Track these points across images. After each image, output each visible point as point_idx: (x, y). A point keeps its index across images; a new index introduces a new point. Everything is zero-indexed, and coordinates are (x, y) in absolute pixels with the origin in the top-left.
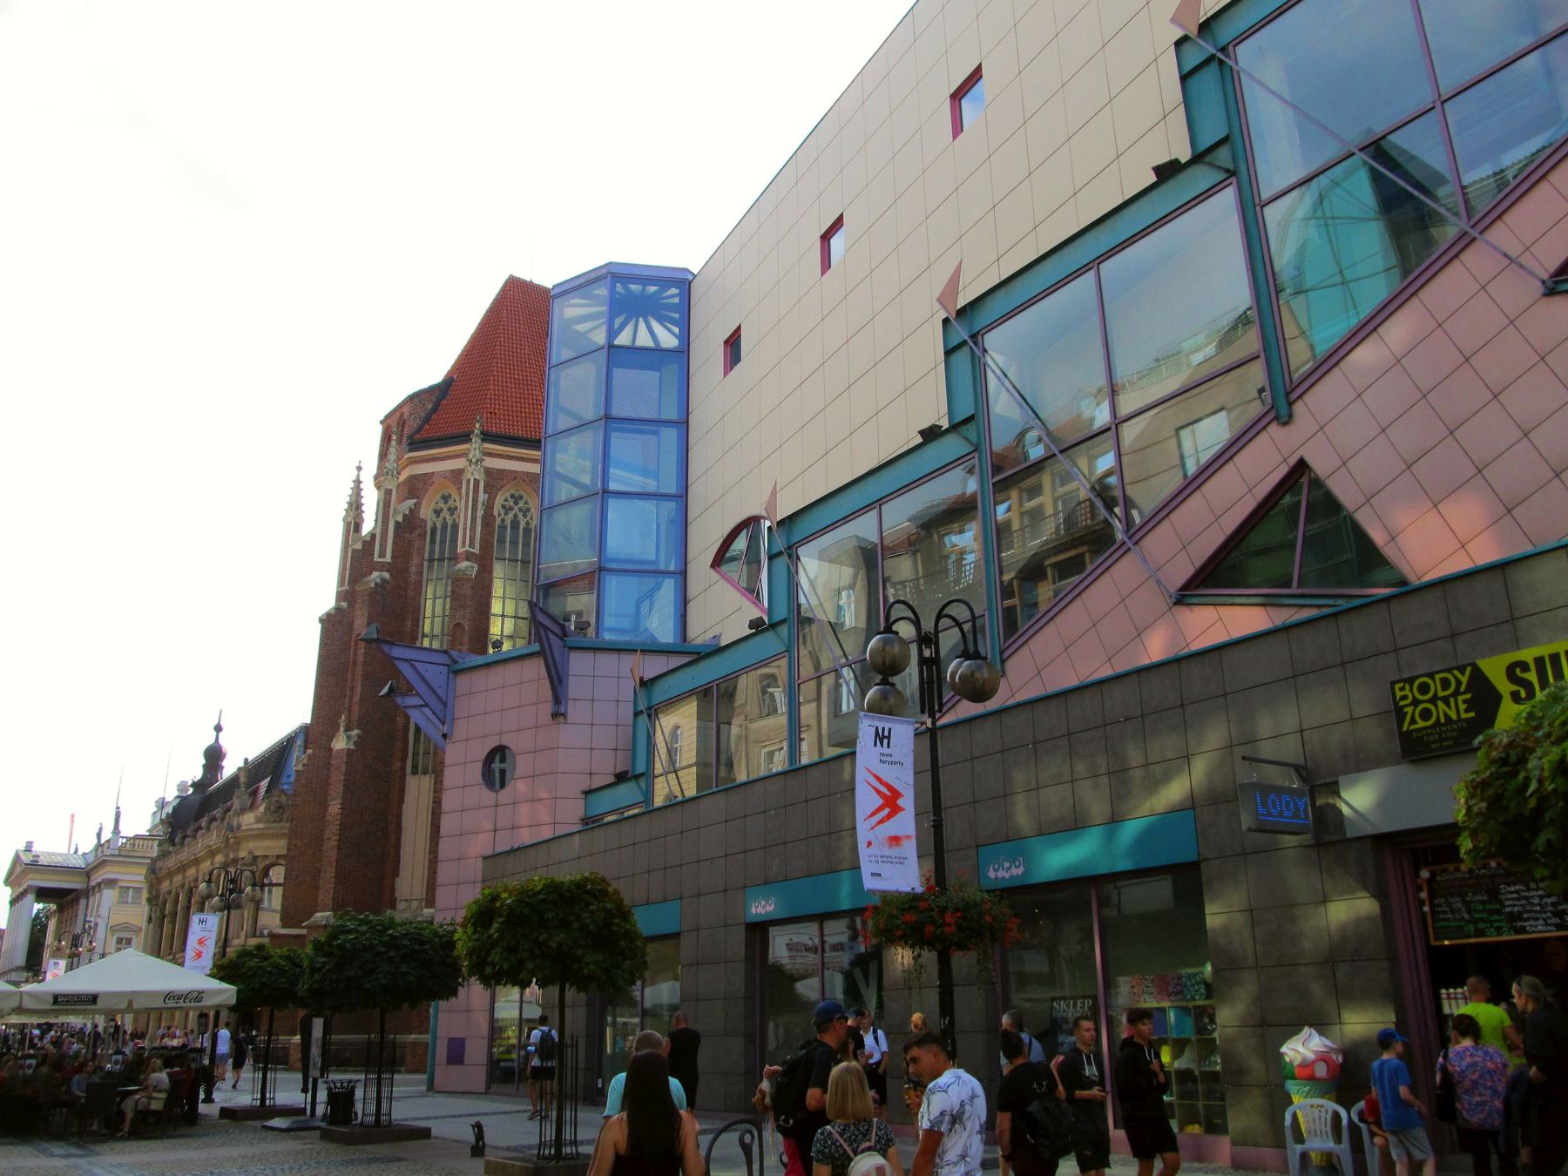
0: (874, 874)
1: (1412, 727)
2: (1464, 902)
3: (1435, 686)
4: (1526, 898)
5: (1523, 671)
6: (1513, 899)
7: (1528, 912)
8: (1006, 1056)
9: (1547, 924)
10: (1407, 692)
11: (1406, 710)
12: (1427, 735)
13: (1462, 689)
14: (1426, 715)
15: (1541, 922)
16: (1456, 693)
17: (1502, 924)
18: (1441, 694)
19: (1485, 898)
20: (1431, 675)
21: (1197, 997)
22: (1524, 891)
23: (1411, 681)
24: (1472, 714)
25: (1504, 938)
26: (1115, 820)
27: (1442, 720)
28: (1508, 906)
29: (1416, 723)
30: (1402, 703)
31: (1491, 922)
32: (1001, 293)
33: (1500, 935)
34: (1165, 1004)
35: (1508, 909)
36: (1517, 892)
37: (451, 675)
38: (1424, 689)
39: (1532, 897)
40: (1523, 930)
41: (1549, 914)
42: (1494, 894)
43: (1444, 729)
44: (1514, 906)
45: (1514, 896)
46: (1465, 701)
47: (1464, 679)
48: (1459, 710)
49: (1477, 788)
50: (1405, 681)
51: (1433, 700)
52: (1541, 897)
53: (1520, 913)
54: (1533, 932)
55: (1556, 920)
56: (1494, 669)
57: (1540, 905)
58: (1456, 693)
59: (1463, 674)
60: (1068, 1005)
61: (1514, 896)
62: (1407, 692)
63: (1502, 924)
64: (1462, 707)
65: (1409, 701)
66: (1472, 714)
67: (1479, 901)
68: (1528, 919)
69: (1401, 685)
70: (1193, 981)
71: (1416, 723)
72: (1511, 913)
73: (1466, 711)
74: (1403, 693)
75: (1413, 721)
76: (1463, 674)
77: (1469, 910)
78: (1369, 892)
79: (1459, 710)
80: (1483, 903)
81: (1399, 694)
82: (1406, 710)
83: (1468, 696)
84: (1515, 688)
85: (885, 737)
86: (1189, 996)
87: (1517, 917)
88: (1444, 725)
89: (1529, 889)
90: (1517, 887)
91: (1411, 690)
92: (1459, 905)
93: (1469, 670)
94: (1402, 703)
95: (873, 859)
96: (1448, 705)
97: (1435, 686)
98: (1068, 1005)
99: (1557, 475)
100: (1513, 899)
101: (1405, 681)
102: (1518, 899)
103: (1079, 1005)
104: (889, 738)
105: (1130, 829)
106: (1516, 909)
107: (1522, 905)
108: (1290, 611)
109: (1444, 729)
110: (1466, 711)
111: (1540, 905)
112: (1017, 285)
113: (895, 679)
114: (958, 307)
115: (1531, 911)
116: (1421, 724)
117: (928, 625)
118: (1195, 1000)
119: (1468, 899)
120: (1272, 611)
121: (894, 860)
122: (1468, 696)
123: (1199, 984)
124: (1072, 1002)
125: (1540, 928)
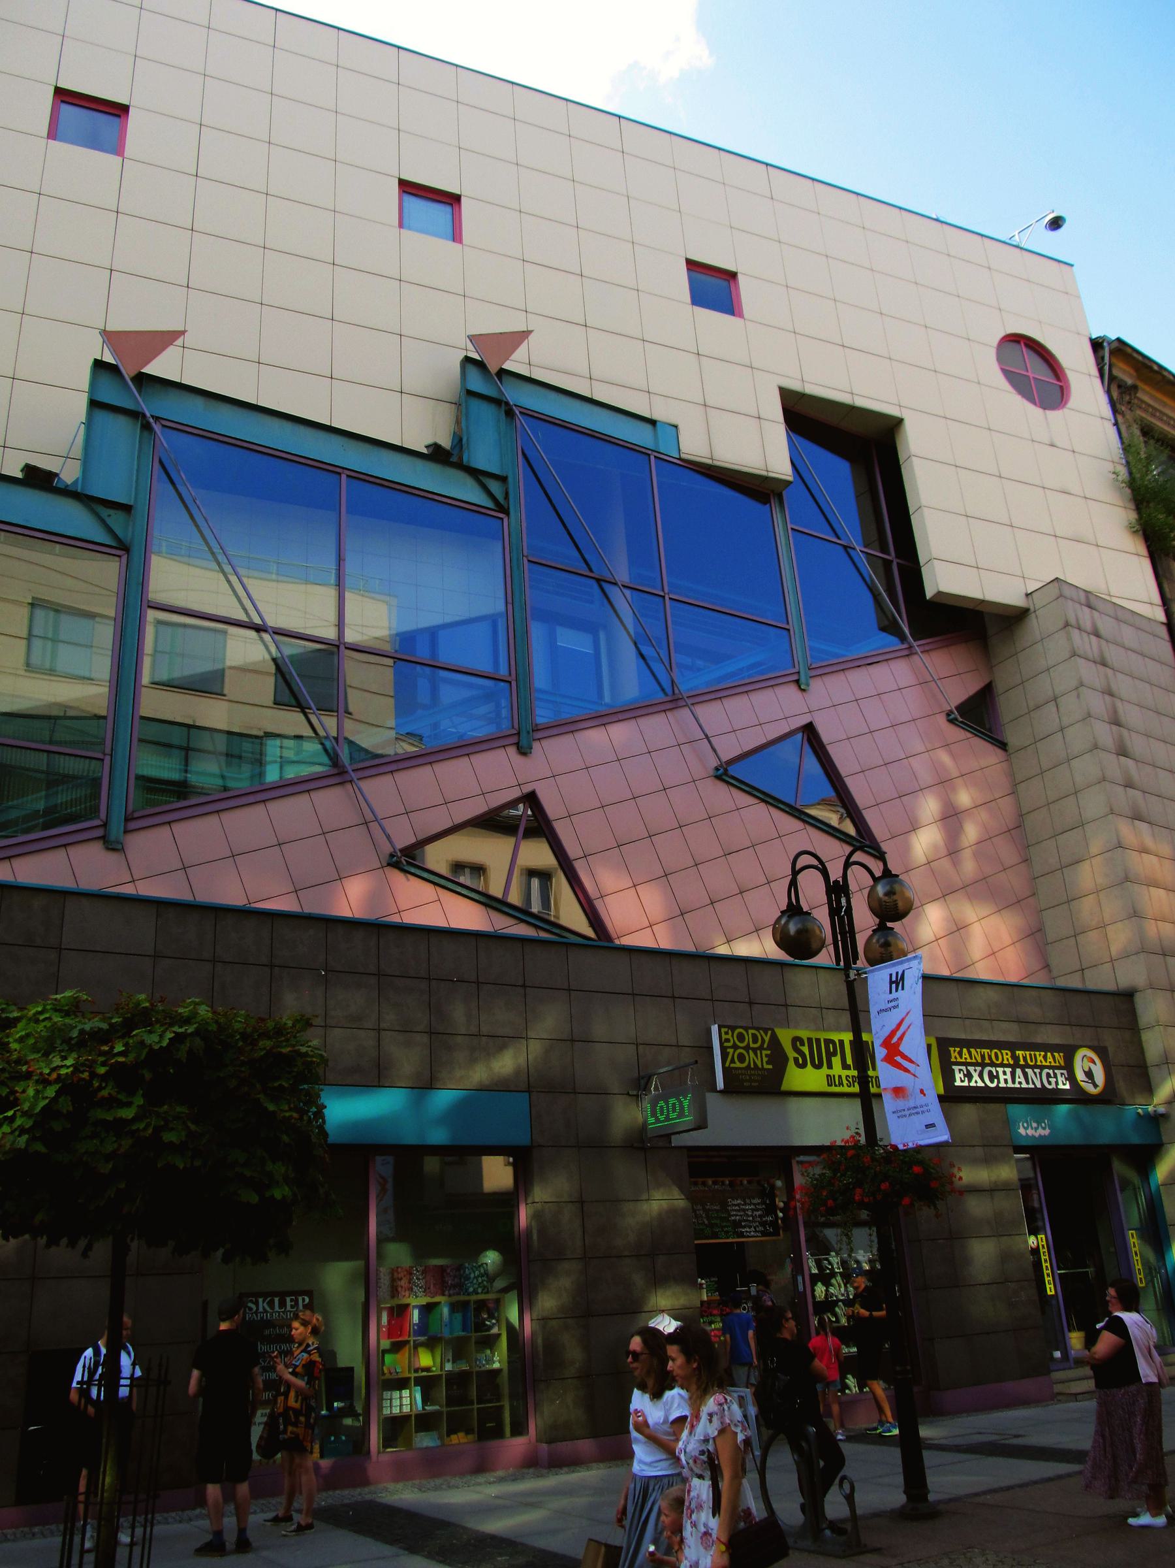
0: (932, 1125)
1: (732, 1065)
2: (704, 1210)
3: (748, 1038)
4: (744, 1210)
5: (801, 1045)
6: (735, 1210)
7: (745, 1221)
8: (1128, 1309)
9: (756, 1231)
10: (729, 1036)
11: (728, 1050)
12: (742, 1075)
13: (765, 1046)
14: (742, 1058)
15: (753, 1229)
16: (761, 1048)
17: (730, 1229)
18: (752, 1045)
19: (718, 1208)
20: (746, 1029)
21: (480, 1290)
22: (743, 1205)
23: (733, 1028)
24: (770, 1067)
25: (730, 1240)
26: (426, 1084)
27: (752, 1066)
28: (733, 1215)
29: (735, 1063)
30: (726, 1044)
31: (722, 1227)
32: (199, 401)
33: (728, 1238)
34: (437, 1299)
35: (733, 1218)
36: (738, 1205)
38: (741, 1038)
39: (747, 1210)
40: (741, 1235)
41: (757, 1224)
42: (724, 1206)
43: (753, 1072)
44: (737, 1215)
45: (737, 1208)
46: (767, 1056)
47: (767, 1039)
48: (761, 1060)
49: (143, 1096)
50: (728, 1027)
51: (747, 1048)
52: (753, 1210)
53: (740, 1221)
54: (749, 1237)
55: (761, 1228)
56: (785, 1036)
57: (752, 1216)
58: (761, 1048)
59: (766, 1035)
60: (271, 1304)
61: (737, 1208)
62: (729, 1036)
63: (730, 1229)
64: (765, 1059)
65: (730, 1044)
66: (770, 1067)
67: (715, 1210)
68: (744, 1227)
69: (726, 1030)
70: (477, 1273)
71: (735, 1063)
72: (734, 1221)
73: (768, 1063)
74: (727, 1037)
75: (733, 1061)
76: (766, 1035)
77: (708, 1217)
78: (685, 1195)
79: (761, 1060)
80: (717, 1211)
81: (724, 1037)
82: (728, 1050)
83: (769, 1052)
84: (797, 1056)
85: (894, 982)
86: (471, 1289)
87: (737, 1224)
88: (753, 1069)
89: (745, 1204)
90: (739, 1202)
91: (733, 1036)
92: (701, 1212)
93: (770, 1032)
94: (726, 1044)
95: (925, 1108)
96: (756, 1054)
97: (748, 1038)
98: (271, 1304)
99: (712, 903)
100: (735, 1210)
101: (728, 1027)
102: (739, 1211)
103: (289, 1303)
104: (891, 982)
105: (443, 1098)
106: (738, 1217)
107: (741, 1215)
108: (512, 921)
109: (753, 1072)
110: (768, 1063)
111: (752, 1216)
112: (226, 411)
113: (896, 926)
114: (145, 370)
115: (747, 1221)
116: (738, 1065)
117: (835, 874)
118: (477, 1293)
119: (708, 1207)
120: (495, 915)
121: (907, 1113)
122: (769, 1052)
123: (483, 1276)
124: (276, 1300)
125: (753, 1233)
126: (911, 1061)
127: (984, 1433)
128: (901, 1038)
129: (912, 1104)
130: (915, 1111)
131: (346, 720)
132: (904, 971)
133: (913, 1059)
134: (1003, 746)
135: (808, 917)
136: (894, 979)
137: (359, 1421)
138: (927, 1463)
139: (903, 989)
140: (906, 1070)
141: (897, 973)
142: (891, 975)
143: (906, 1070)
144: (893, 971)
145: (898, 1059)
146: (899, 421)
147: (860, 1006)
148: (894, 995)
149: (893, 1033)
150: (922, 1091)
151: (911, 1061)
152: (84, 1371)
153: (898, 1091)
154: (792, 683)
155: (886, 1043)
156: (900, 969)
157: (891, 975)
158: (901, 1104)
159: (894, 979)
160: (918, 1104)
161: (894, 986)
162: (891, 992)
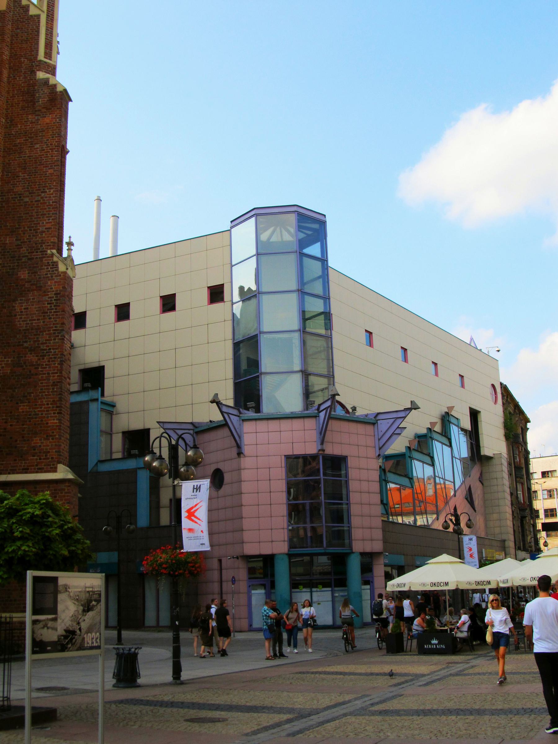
37: (241, 421)
104: (194, 488)
117: (174, 442)
126: (199, 519)
127: (296, 673)
128: (196, 510)
129: (196, 535)
130: (196, 538)
131: (248, 427)
132: (200, 485)
133: (201, 519)
134: (483, 484)
135: (163, 460)
136: (195, 487)
137: (65, 642)
138: (546, 705)
139: (200, 491)
140: (196, 522)
141: (197, 485)
142: (194, 486)
143: (196, 522)
144: (195, 484)
145: (193, 518)
146: (480, 412)
147: (461, 549)
148: (470, 542)
149: (192, 508)
150: (202, 531)
151: (199, 519)
152: (18, 617)
153: (190, 530)
154: (78, 346)
155: (188, 511)
156: (199, 484)
157: (194, 486)
158: (191, 535)
159: (195, 487)
160: (199, 535)
161: (195, 490)
162: (193, 492)
